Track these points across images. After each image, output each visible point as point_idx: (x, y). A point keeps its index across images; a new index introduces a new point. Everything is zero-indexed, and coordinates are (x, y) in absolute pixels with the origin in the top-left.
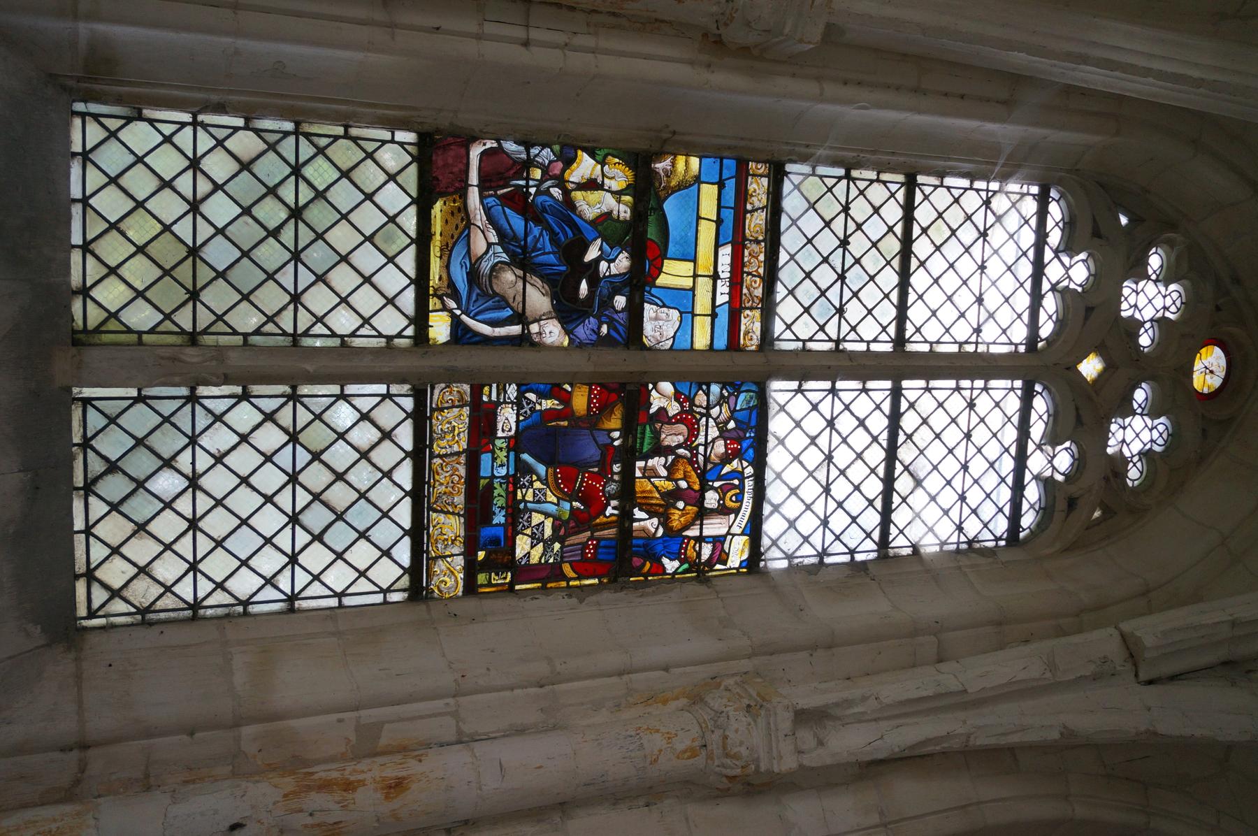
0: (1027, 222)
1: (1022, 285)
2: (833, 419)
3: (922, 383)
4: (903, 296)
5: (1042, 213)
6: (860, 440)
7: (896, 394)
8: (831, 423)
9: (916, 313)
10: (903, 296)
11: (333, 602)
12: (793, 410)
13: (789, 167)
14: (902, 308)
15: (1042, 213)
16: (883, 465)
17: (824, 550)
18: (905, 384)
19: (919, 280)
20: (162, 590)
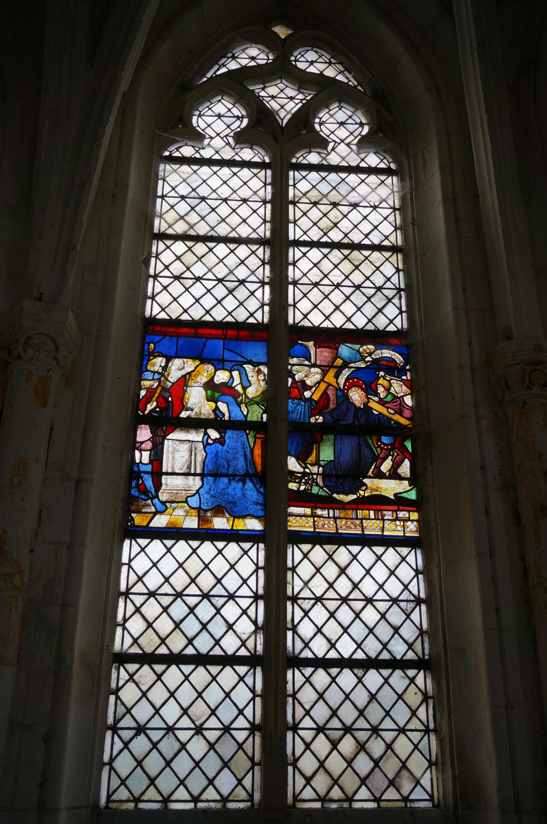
0: (324, 179)
1: (343, 180)
2: (355, 286)
3: (291, 226)
4: (325, 245)
5: (310, 167)
6: (367, 268)
7: (297, 243)
8: (358, 287)
9: (244, 231)
10: (325, 245)
11: (106, 758)
12: (308, 310)
13: (147, 313)
14: (239, 241)
15: (310, 167)
16: (322, 249)
17: (396, 289)
18: (291, 237)
19: (223, 230)
20: (336, 786)
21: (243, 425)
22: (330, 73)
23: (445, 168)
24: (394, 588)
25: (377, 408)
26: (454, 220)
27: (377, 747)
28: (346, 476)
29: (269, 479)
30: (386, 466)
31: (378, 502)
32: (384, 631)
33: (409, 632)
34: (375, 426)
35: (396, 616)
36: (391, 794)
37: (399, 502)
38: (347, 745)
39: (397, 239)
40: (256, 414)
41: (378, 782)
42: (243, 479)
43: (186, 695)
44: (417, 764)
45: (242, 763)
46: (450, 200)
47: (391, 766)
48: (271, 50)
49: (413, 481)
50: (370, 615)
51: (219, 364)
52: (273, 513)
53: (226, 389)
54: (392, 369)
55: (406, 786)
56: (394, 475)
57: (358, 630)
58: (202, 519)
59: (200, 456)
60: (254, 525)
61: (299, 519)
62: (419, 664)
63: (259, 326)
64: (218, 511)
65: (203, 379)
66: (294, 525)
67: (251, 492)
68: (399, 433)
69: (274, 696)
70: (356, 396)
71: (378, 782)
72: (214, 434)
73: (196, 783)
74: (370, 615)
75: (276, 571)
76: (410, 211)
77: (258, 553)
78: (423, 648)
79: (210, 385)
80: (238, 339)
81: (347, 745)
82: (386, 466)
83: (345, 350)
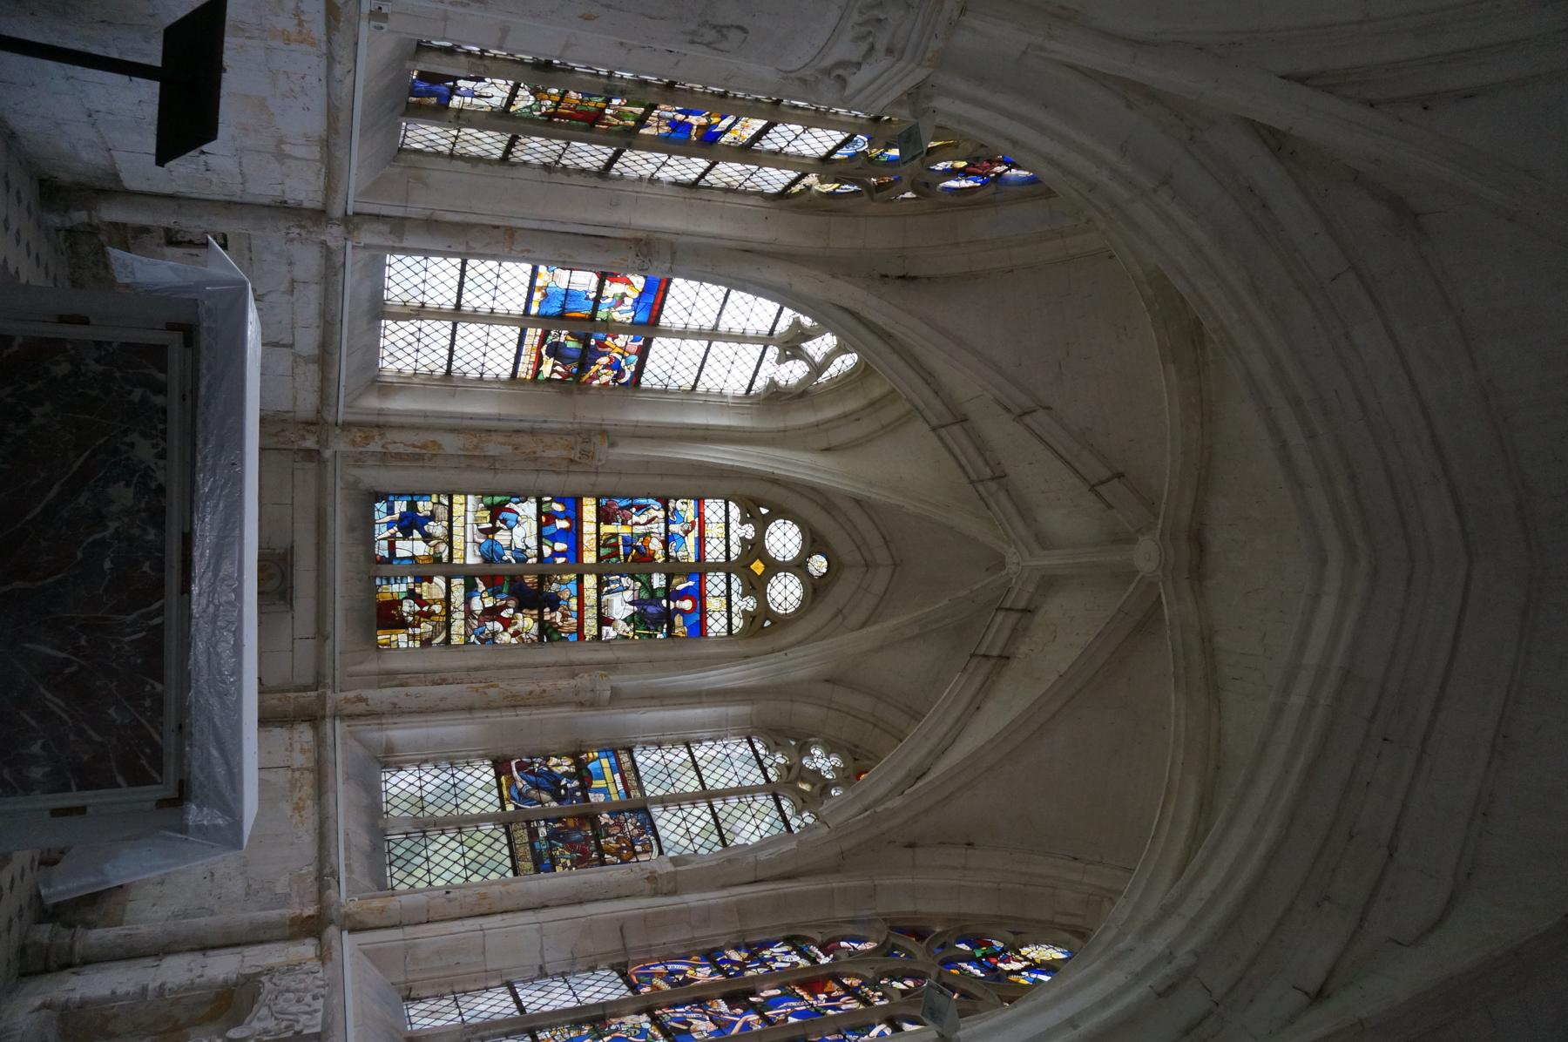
12: (659, 346)
21: (595, 309)
22: (826, 374)
23: (729, 428)
24: (489, 365)
25: (594, 368)
26: (694, 428)
27: (409, 350)
28: (556, 351)
29: (562, 318)
30: (559, 368)
31: (539, 362)
32: (467, 359)
33: (466, 368)
34: (584, 365)
35: (475, 364)
36: (386, 353)
37: (537, 372)
38: (411, 339)
39: (701, 388)
40: (601, 315)
41: (393, 349)
42: (563, 307)
43: (443, 277)
44: (399, 365)
45: (406, 297)
46: (707, 428)
47: (399, 354)
48: (531, 609)
49: (549, 380)
50: (477, 354)
51: (637, 301)
52: (542, 318)
53: (621, 302)
54: (616, 378)
55: (390, 359)
56: (553, 371)
57: (469, 349)
58: (540, 289)
59: (580, 289)
60: (534, 310)
61: (533, 335)
62: (449, 371)
63: (658, 318)
64: (545, 295)
65: (629, 292)
66: (531, 331)
67: (554, 309)
68: (578, 376)
69: (439, 314)
70: (604, 360)
71: (393, 349)
72: (592, 296)
73: (398, 278)
74: (477, 354)
75: (507, 320)
76: (718, 401)
77: (518, 310)
78: (456, 373)
79: (624, 295)
80: (652, 310)
81: (411, 339)
82: (559, 368)
83: (634, 358)
